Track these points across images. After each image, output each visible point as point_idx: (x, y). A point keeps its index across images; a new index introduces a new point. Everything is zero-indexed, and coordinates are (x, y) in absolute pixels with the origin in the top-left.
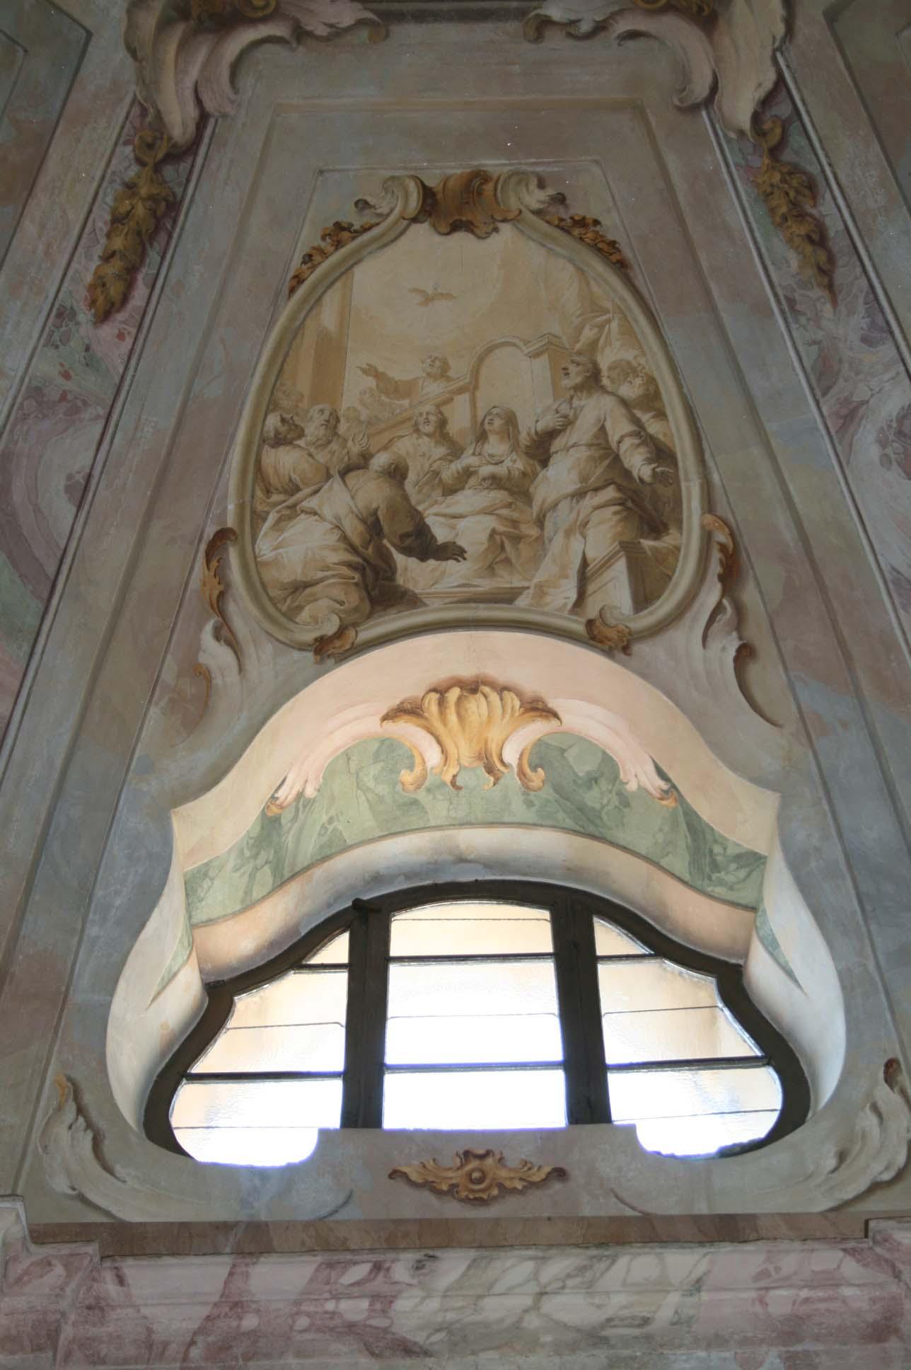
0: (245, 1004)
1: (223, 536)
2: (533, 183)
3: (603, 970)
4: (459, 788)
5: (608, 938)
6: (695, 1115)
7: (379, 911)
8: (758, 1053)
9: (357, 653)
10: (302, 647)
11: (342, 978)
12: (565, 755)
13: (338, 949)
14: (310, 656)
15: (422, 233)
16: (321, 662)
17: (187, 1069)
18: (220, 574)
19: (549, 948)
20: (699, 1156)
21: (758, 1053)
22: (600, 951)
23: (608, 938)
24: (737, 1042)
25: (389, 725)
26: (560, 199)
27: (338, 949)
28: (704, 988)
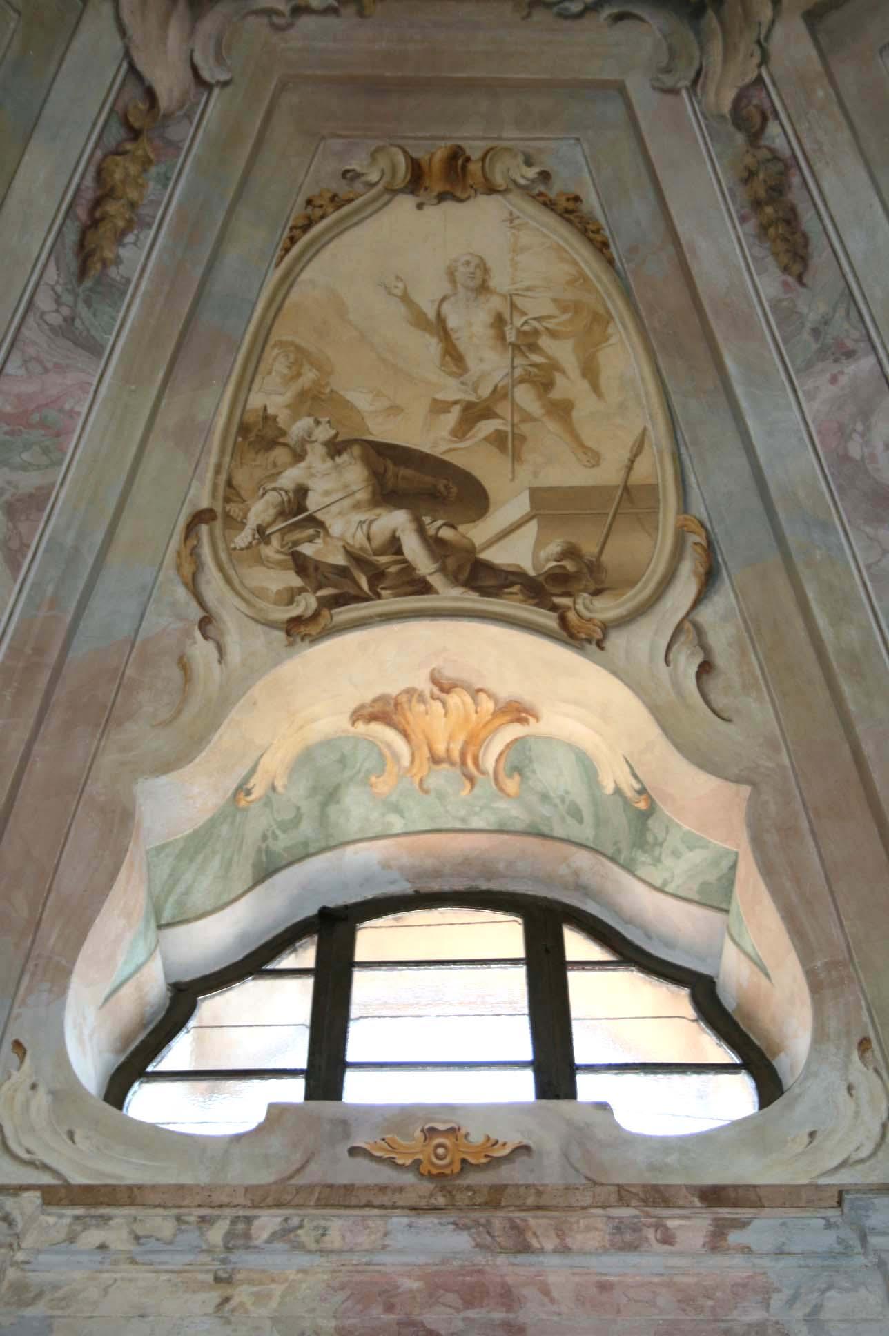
0: (210, 1007)
1: (201, 517)
2: (521, 159)
3: (573, 977)
4: (427, 792)
5: (577, 945)
6: (673, 1115)
7: (345, 919)
8: (737, 1060)
9: (328, 634)
10: (272, 625)
11: (308, 983)
12: (545, 1250)
13: (306, 956)
14: (280, 635)
15: (406, 203)
16: (291, 644)
17: (145, 1069)
18: (195, 553)
19: (520, 952)
20: (755, 858)
21: (737, 1060)
22: (570, 956)
23: (577, 945)
24: (719, 1052)
25: (361, 727)
26: (545, 176)
27: (306, 956)
28: (679, 1000)
